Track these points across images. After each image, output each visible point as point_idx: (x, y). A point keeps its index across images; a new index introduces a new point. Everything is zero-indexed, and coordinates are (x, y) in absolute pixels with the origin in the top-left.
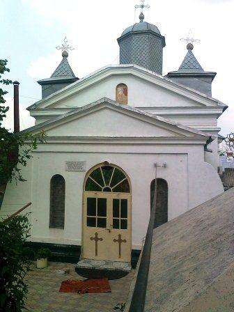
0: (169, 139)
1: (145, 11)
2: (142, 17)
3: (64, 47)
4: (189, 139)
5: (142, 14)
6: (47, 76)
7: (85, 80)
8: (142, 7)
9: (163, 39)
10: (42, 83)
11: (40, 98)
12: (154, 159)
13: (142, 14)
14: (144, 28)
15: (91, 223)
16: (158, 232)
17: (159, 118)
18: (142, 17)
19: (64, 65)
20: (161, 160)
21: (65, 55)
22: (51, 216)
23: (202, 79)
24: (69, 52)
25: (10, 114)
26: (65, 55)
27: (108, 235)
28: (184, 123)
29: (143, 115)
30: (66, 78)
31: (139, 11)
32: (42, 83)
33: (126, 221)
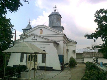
0: (44, 41)
1: (56, 8)
2: (55, 10)
3: (29, 21)
4: (49, 41)
5: (55, 9)
6: (25, 28)
7: (34, 28)
8: (55, 7)
9: (60, 16)
10: (23, 30)
11: (23, 33)
12: (43, 46)
13: (55, 9)
14: (55, 14)
15: (29, 60)
16: (54, 68)
17: (44, 37)
18: (55, 10)
19: (29, 25)
20: (44, 46)
21: (29, 23)
22: (21, 58)
23: (60, 28)
24: (31, 22)
25: (14, 37)
26: (29, 23)
27: (33, 63)
28: (49, 38)
29: (40, 36)
30: (28, 28)
31: (54, 9)
32: (23, 30)
33: (37, 60)
